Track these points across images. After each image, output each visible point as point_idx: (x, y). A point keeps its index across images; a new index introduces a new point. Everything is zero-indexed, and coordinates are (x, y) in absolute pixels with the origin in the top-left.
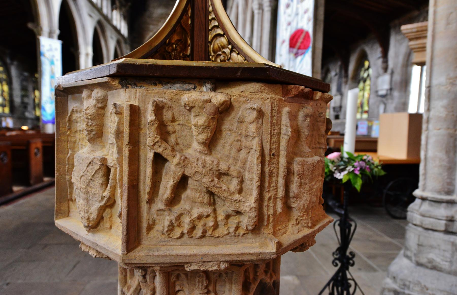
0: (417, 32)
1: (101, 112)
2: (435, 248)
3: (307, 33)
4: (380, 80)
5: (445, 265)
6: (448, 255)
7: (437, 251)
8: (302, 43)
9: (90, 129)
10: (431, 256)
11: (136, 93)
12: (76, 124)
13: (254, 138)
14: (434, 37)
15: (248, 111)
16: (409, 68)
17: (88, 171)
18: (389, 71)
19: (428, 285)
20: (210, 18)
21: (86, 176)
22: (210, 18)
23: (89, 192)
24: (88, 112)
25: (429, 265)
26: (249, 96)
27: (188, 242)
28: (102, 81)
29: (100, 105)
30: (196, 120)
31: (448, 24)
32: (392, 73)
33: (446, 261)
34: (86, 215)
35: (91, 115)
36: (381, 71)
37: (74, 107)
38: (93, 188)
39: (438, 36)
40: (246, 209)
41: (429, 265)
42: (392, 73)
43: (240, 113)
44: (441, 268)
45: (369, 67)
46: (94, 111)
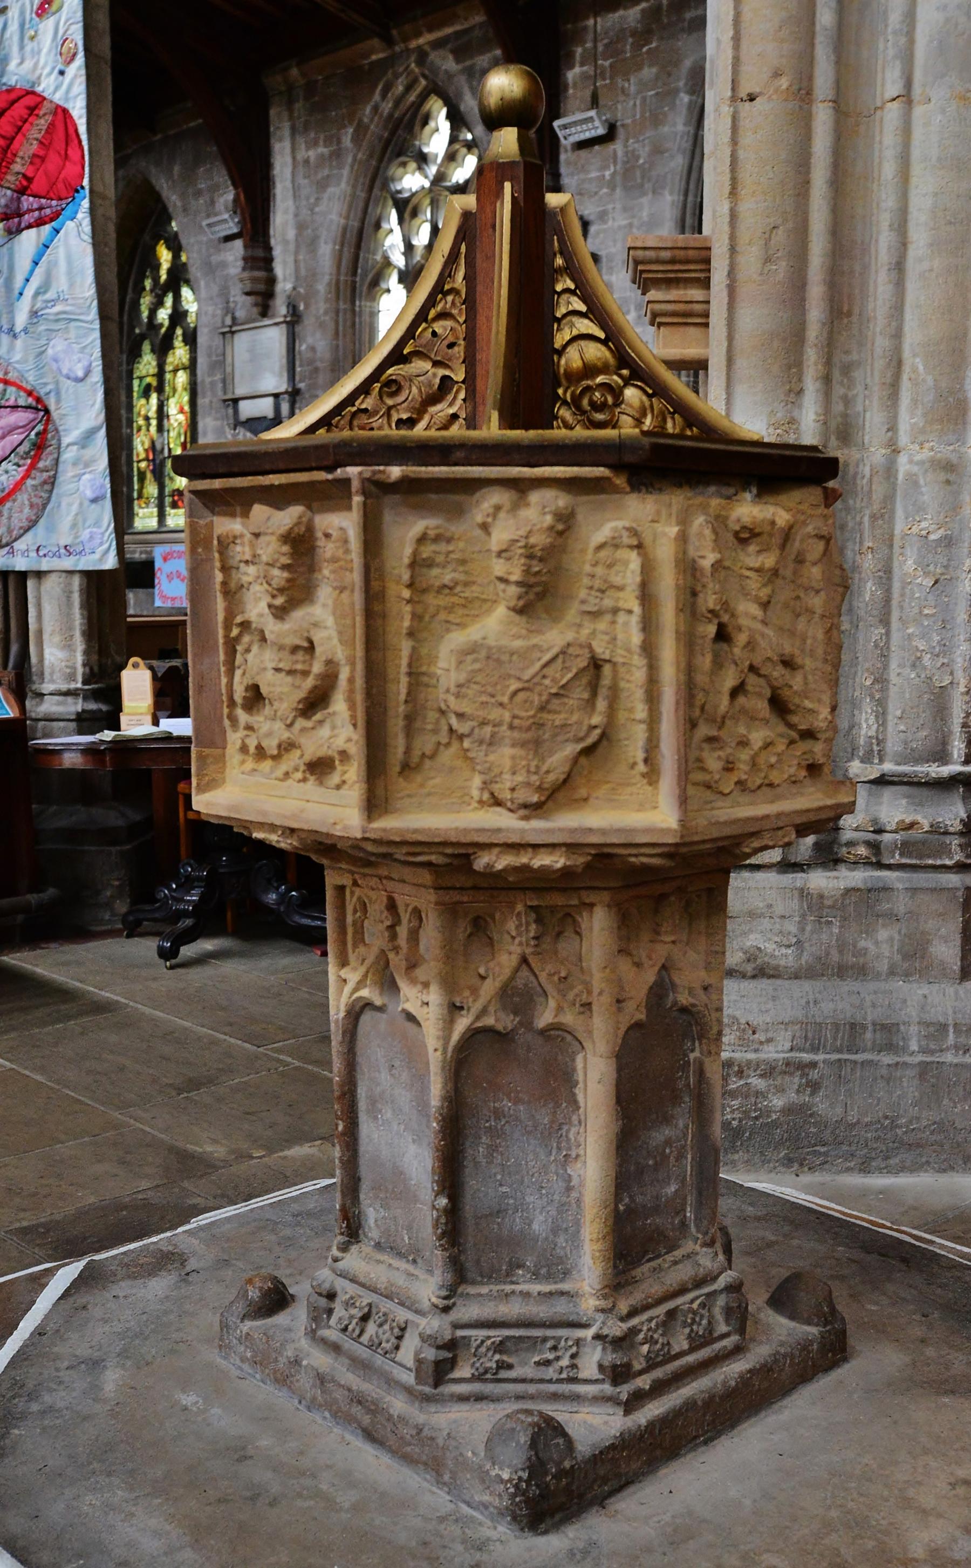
0: (673, 261)
1: (560, 541)
2: (762, 915)
3: (63, 113)
4: (242, 342)
5: (786, 958)
6: (792, 927)
7: (766, 923)
8: (38, 159)
9: (533, 580)
10: (753, 940)
11: (670, 505)
12: (425, 570)
13: (818, 592)
14: (732, 290)
15: (810, 541)
16: (362, 304)
17: (544, 677)
18: (281, 308)
19: (757, 1019)
20: (559, 288)
21: (538, 689)
22: (559, 288)
23: (543, 725)
24: (532, 540)
25: (749, 968)
26: (809, 512)
27: (740, 799)
28: (589, 476)
29: (560, 527)
30: (760, 559)
31: (768, 260)
32: (294, 321)
33: (789, 946)
34: (534, 778)
35: (542, 550)
36: (243, 305)
37: (427, 528)
38: (559, 712)
39: (743, 291)
40: (821, 724)
41: (749, 968)
42: (294, 321)
43: (797, 544)
44: (776, 968)
45: (178, 276)
46: (548, 540)
